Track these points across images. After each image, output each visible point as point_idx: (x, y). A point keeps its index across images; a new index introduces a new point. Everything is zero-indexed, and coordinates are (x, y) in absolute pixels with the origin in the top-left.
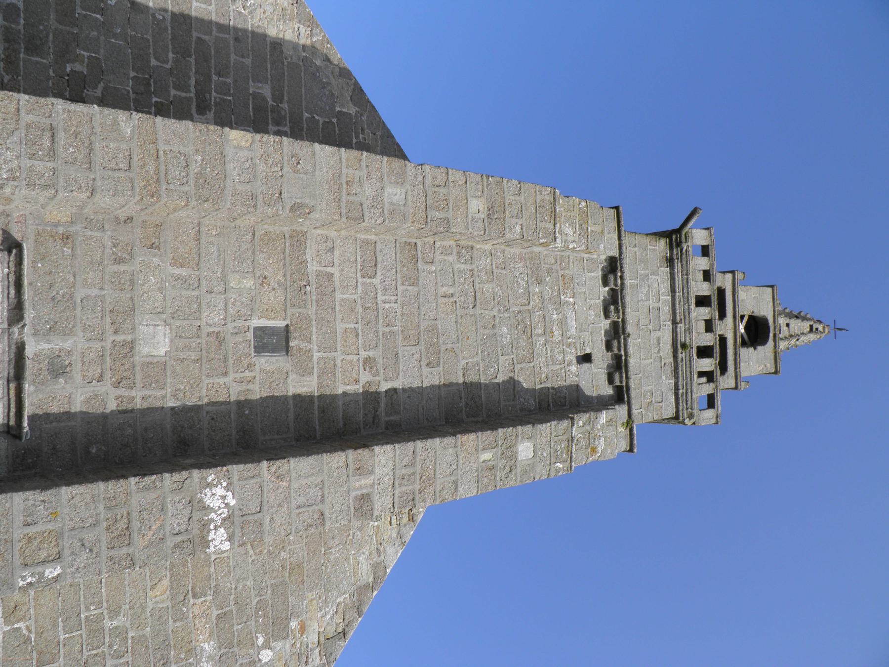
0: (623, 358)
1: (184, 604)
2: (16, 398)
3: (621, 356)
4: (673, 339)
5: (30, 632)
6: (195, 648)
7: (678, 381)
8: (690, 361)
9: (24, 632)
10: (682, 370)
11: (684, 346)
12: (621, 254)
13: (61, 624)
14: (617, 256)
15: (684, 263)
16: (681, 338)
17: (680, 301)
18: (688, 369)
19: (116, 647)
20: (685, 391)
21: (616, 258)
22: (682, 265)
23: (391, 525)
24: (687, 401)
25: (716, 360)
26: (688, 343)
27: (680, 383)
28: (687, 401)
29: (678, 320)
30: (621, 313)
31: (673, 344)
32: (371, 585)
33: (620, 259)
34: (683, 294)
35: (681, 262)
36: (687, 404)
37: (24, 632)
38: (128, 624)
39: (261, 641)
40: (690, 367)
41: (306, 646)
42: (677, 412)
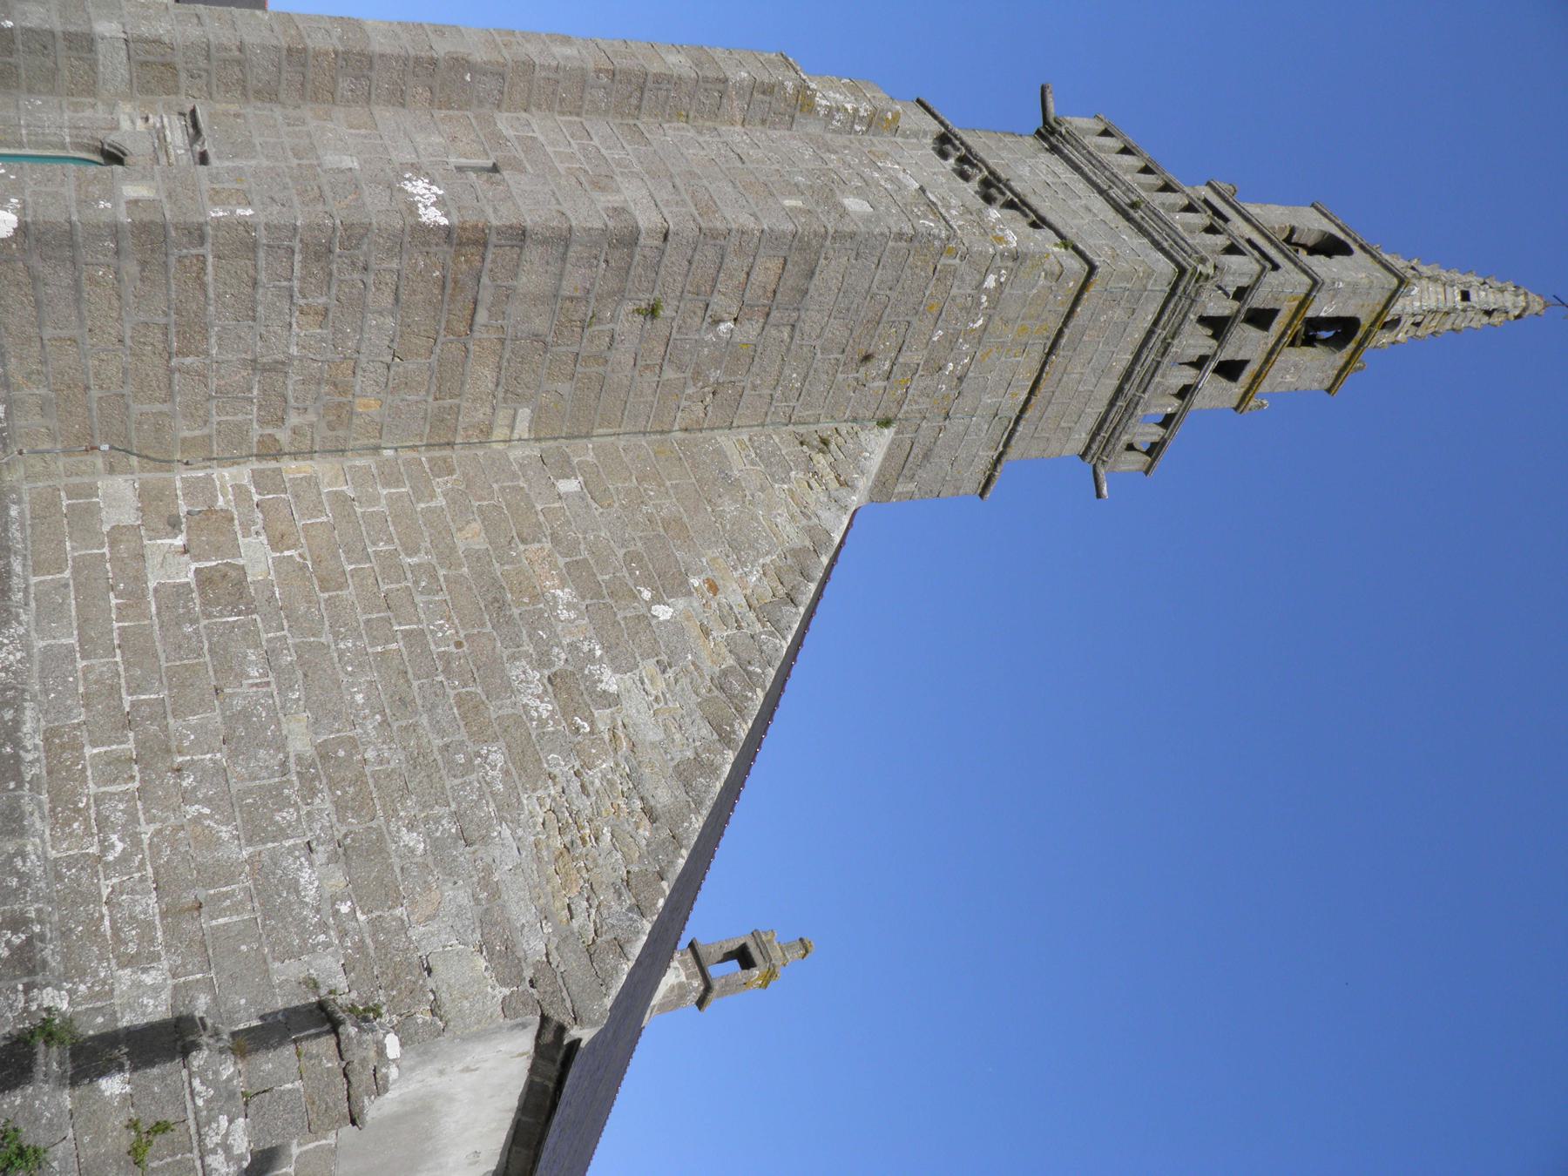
0: (1016, 200)
1: (511, 549)
2: (512, 1132)
3: (1012, 200)
4: (1112, 206)
5: (305, 559)
6: (543, 594)
7: (1153, 237)
8: (1155, 214)
9: (298, 559)
10: (1150, 226)
11: (1134, 205)
12: (942, 123)
13: (342, 555)
14: (943, 130)
15: (1074, 143)
16: (1124, 200)
17: (1095, 174)
18: (1159, 222)
19: (423, 584)
20: (1171, 242)
21: (944, 134)
22: (1072, 146)
23: (812, 489)
24: (1182, 249)
25: (1206, 212)
26: (1135, 198)
27: (1157, 237)
28: (1182, 249)
29: (1105, 187)
30: (980, 164)
31: (1117, 210)
32: (812, 549)
33: (949, 131)
34: (1094, 166)
35: (1068, 143)
36: (1185, 252)
37: (298, 559)
38: (434, 562)
39: (647, 595)
40: (1161, 220)
41: (727, 608)
42: (1178, 264)
